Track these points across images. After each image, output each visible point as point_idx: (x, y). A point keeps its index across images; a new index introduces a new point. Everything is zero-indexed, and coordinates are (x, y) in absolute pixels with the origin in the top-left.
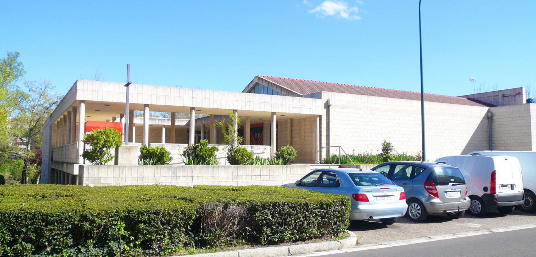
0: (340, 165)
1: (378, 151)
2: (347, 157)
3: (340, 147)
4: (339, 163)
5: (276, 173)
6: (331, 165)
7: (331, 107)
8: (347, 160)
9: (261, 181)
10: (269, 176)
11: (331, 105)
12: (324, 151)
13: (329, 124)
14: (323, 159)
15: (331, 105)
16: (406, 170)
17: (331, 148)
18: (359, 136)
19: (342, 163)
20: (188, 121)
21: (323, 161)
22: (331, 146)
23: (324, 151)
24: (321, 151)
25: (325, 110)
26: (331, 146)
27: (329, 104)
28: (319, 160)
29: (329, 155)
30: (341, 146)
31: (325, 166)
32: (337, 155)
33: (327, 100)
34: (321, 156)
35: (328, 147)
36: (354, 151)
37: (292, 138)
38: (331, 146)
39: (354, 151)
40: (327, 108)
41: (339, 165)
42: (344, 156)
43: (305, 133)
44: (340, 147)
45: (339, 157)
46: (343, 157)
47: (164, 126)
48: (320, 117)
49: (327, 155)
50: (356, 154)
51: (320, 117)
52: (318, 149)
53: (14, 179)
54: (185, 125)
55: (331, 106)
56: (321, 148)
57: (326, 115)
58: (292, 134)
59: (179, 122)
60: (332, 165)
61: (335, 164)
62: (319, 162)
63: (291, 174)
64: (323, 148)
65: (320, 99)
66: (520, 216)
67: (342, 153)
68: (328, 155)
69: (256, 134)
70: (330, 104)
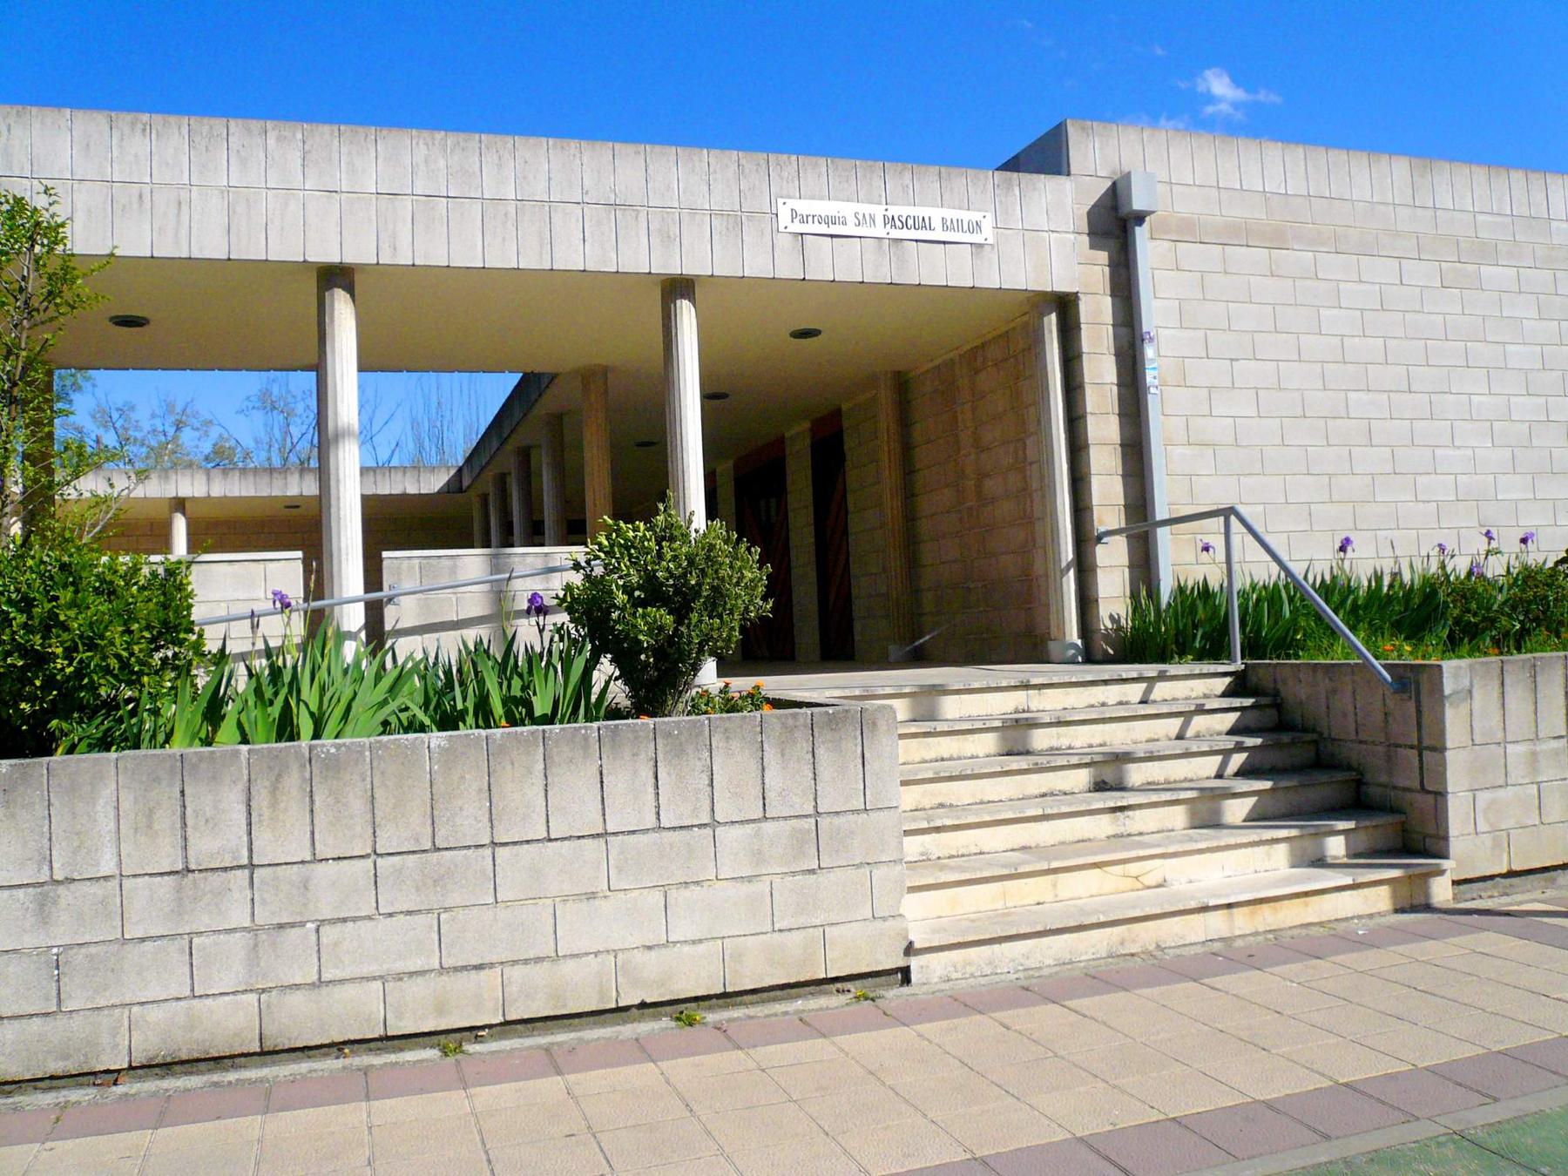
0: (1238, 665)
1: (1524, 541)
2: (1291, 600)
3: (1228, 513)
4: (1230, 658)
5: (468, 821)
6: (1162, 677)
7: (1141, 234)
8: (1294, 620)
9: (252, 930)
10: (369, 863)
11: (1140, 218)
12: (1112, 559)
13: (1134, 358)
14: (1109, 625)
15: (1140, 218)
16: (1106, 253)
17: (1163, 534)
18: (1208, 358)
19: (1253, 648)
20: (452, 472)
21: (1106, 637)
22: (1159, 517)
23: (1112, 559)
24: (1085, 568)
25: (1103, 256)
26: (1161, 513)
27: (1124, 211)
28: (1073, 634)
29: (1153, 594)
30: (1242, 509)
31: (1106, 682)
32: (1214, 585)
33: (1109, 183)
34: (1087, 602)
35: (1140, 528)
36: (1343, 549)
37: (913, 495)
38: (1159, 517)
39: (1343, 549)
40: (1112, 243)
41: (1231, 668)
42: (1271, 596)
43: (980, 448)
44: (1233, 518)
45: (1229, 601)
46: (1258, 600)
47: (180, 504)
48: (1065, 305)
49: (1134, 596)
50: (1363, 566)
51: (1065, 305)
52: (1068, 552)
53: (513, 781)
54: (439, 492)
55: (1146, 225)
56: (1085, 539)
57: (1113, 295)
58: (908, 470)
59: (408, 475)
60: (1172, 669)
61: (1200, 657)
62: (1074, 646)
63: (665, 823)
64: (1099, 539)
65: (1059, 173)
66: (296, 132)
67: (1256, 569)
68: (1144, 593)
69: (763, 503)
70: (1138, 204)
